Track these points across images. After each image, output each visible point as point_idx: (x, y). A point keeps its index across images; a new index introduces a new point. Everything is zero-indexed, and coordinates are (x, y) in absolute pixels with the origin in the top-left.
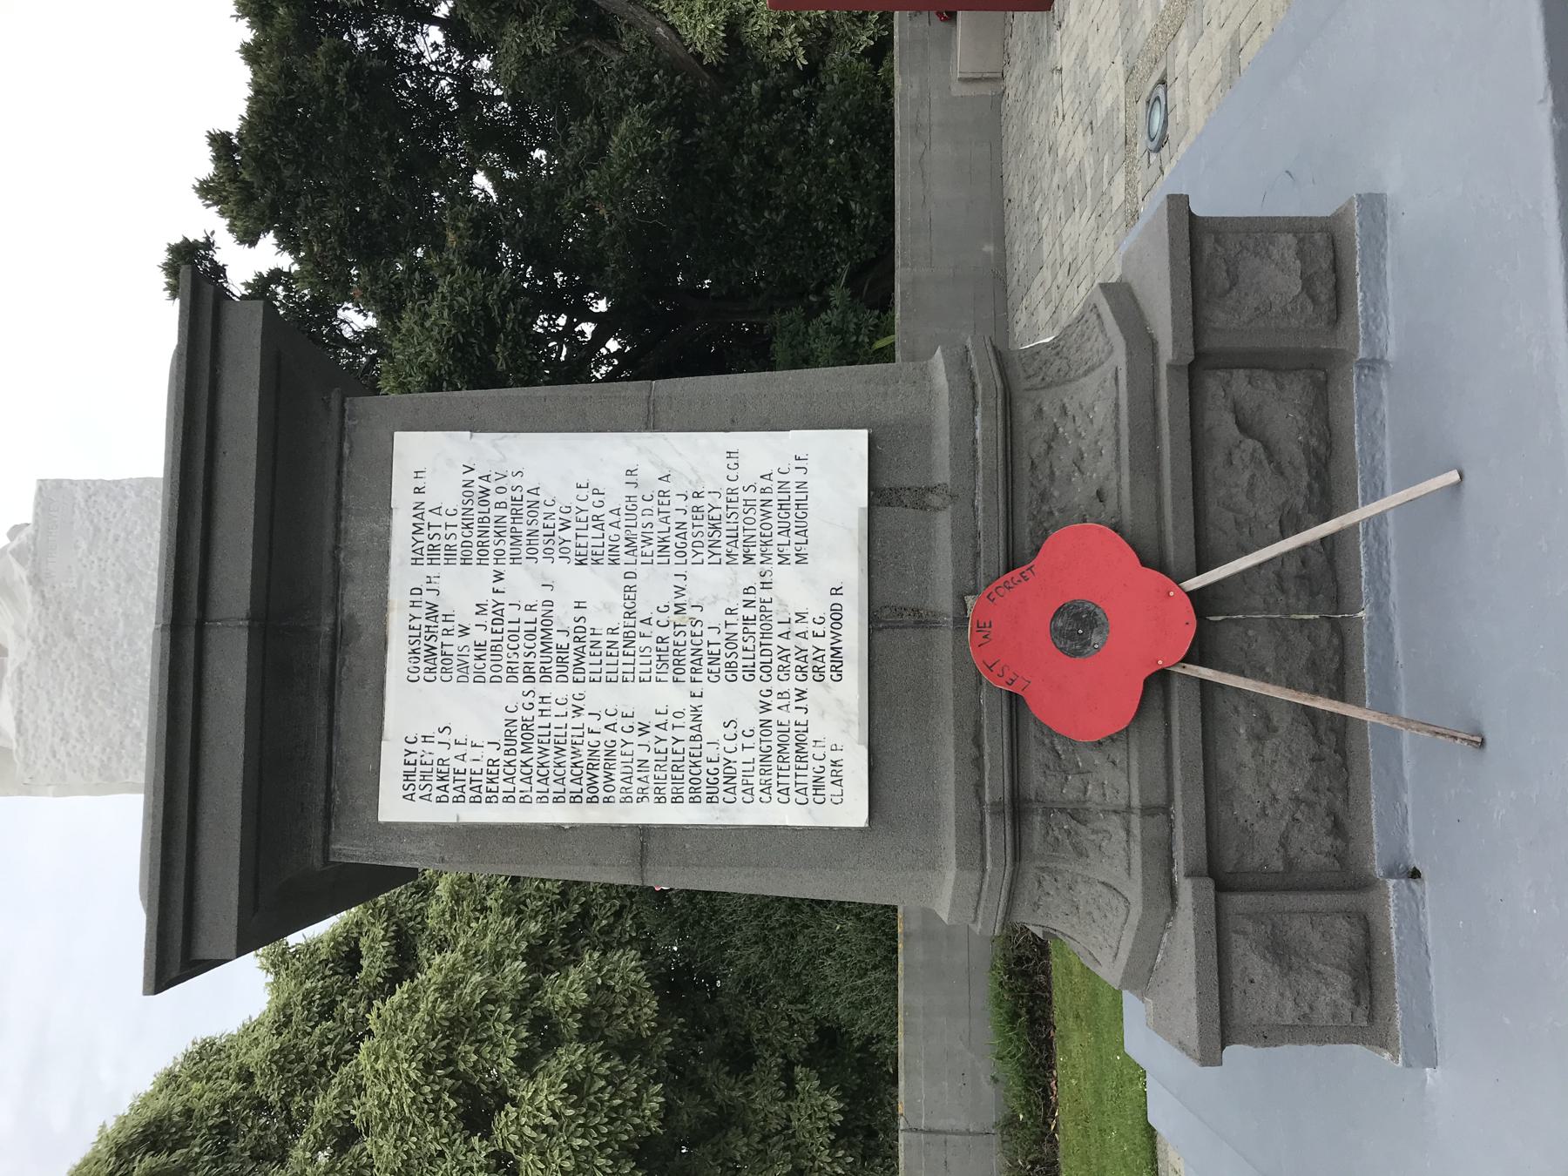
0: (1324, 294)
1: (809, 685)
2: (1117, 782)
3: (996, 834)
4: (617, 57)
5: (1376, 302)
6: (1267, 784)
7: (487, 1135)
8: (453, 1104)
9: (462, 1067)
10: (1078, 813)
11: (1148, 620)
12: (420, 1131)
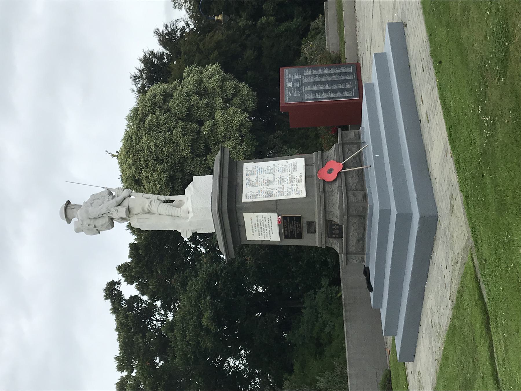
0: (357, 136)
3: (322, 195)
10: (332, 191)
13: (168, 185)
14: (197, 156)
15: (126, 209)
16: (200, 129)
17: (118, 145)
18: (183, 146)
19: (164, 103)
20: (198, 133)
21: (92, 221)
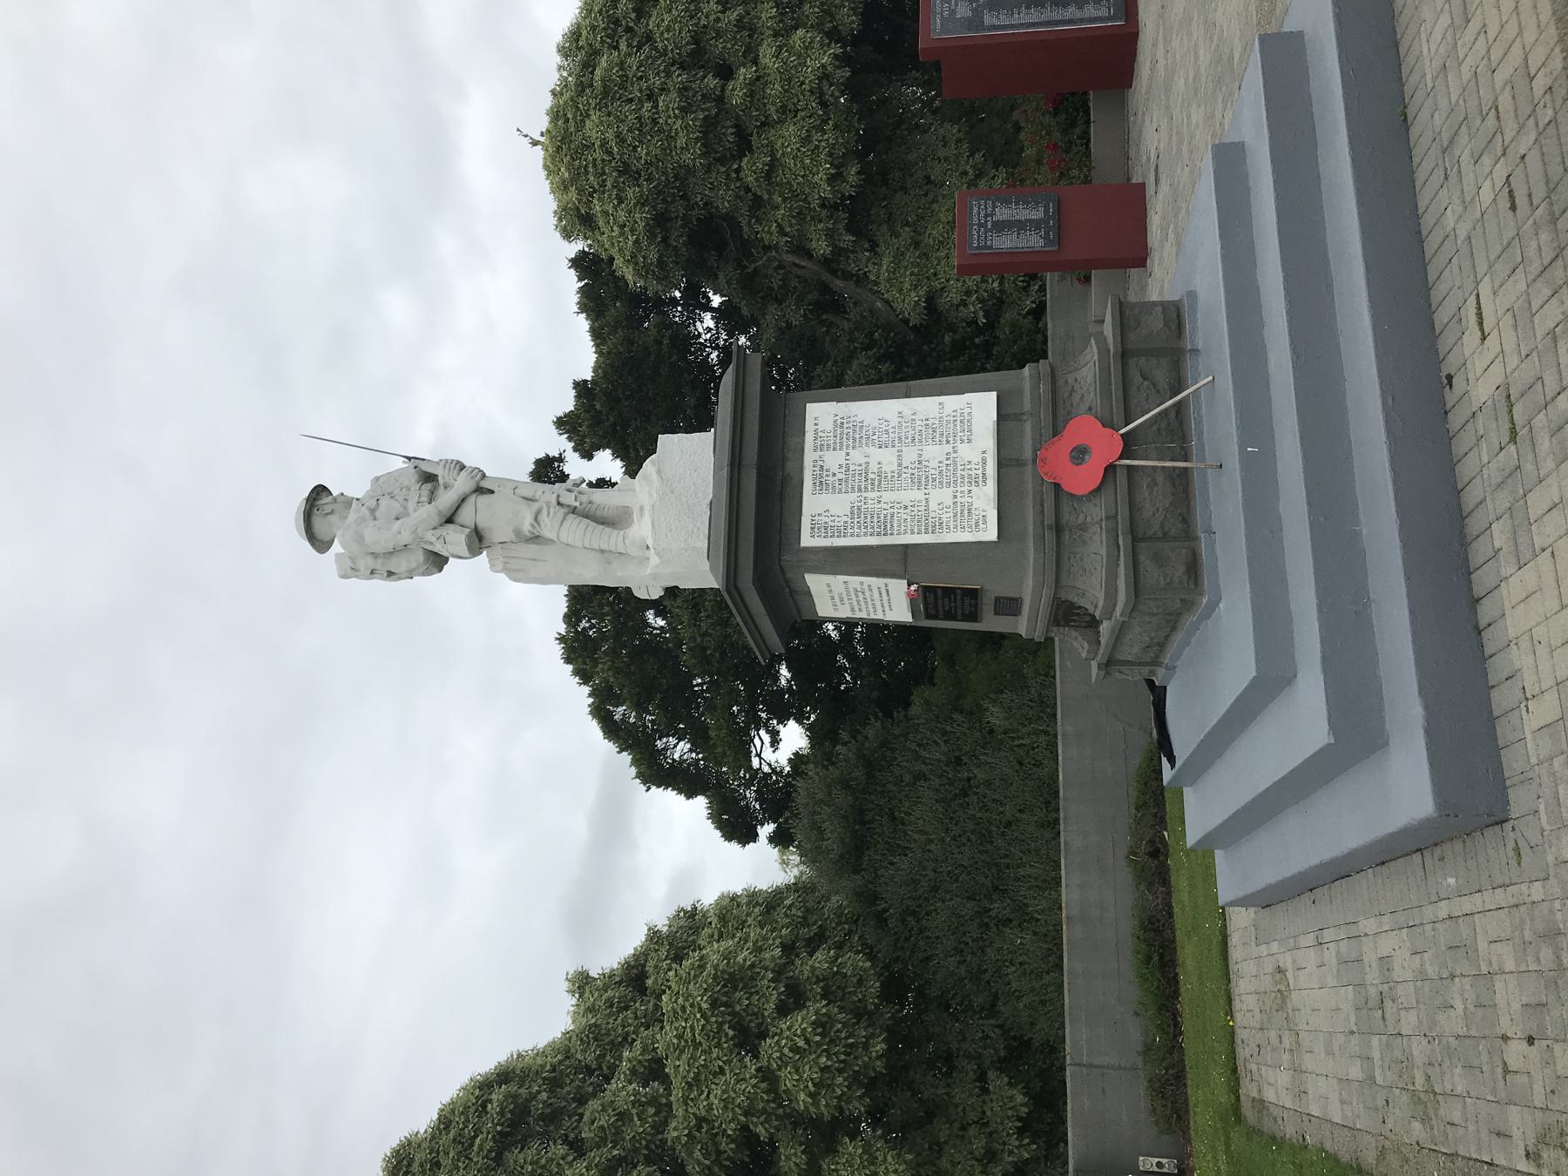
1: (973, 488)
2: (1096, 512)
3: (1050, 537)
4: (846, 325)
5: (1194, 329)
6: (1154, 503)
7: (756, 1056)
8: (731, 1033)
9: (738, 1008)
10: (1083, 528)
11: (1105, 446)
12: (708, 1052)
13: (652, 236)
14: (717, 160)
15: (469, 537)
16: (723, 91)
17: (540, 123)
18: (682, 141)
19: (639, 18)
20: (720, 99)
21: (379, 561)
